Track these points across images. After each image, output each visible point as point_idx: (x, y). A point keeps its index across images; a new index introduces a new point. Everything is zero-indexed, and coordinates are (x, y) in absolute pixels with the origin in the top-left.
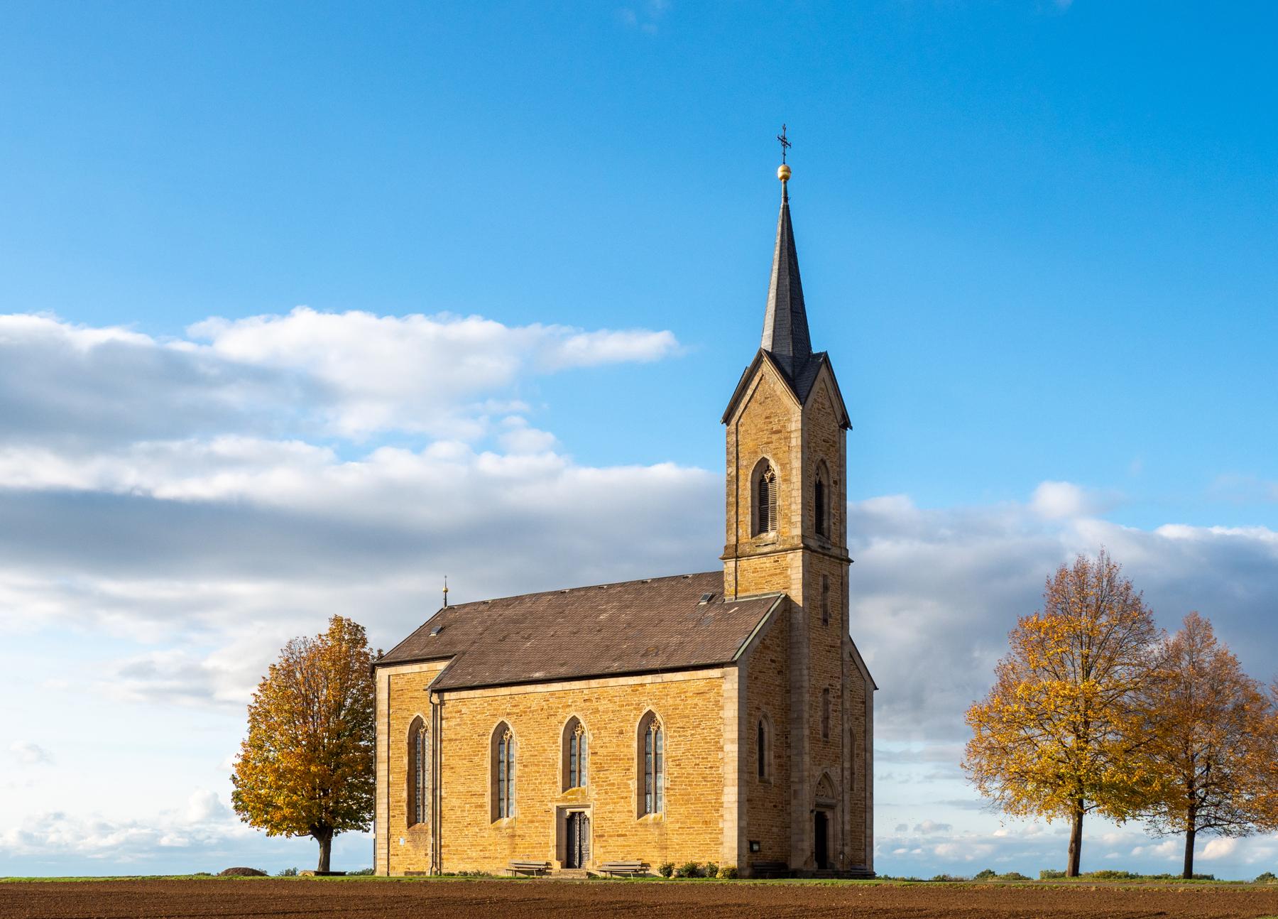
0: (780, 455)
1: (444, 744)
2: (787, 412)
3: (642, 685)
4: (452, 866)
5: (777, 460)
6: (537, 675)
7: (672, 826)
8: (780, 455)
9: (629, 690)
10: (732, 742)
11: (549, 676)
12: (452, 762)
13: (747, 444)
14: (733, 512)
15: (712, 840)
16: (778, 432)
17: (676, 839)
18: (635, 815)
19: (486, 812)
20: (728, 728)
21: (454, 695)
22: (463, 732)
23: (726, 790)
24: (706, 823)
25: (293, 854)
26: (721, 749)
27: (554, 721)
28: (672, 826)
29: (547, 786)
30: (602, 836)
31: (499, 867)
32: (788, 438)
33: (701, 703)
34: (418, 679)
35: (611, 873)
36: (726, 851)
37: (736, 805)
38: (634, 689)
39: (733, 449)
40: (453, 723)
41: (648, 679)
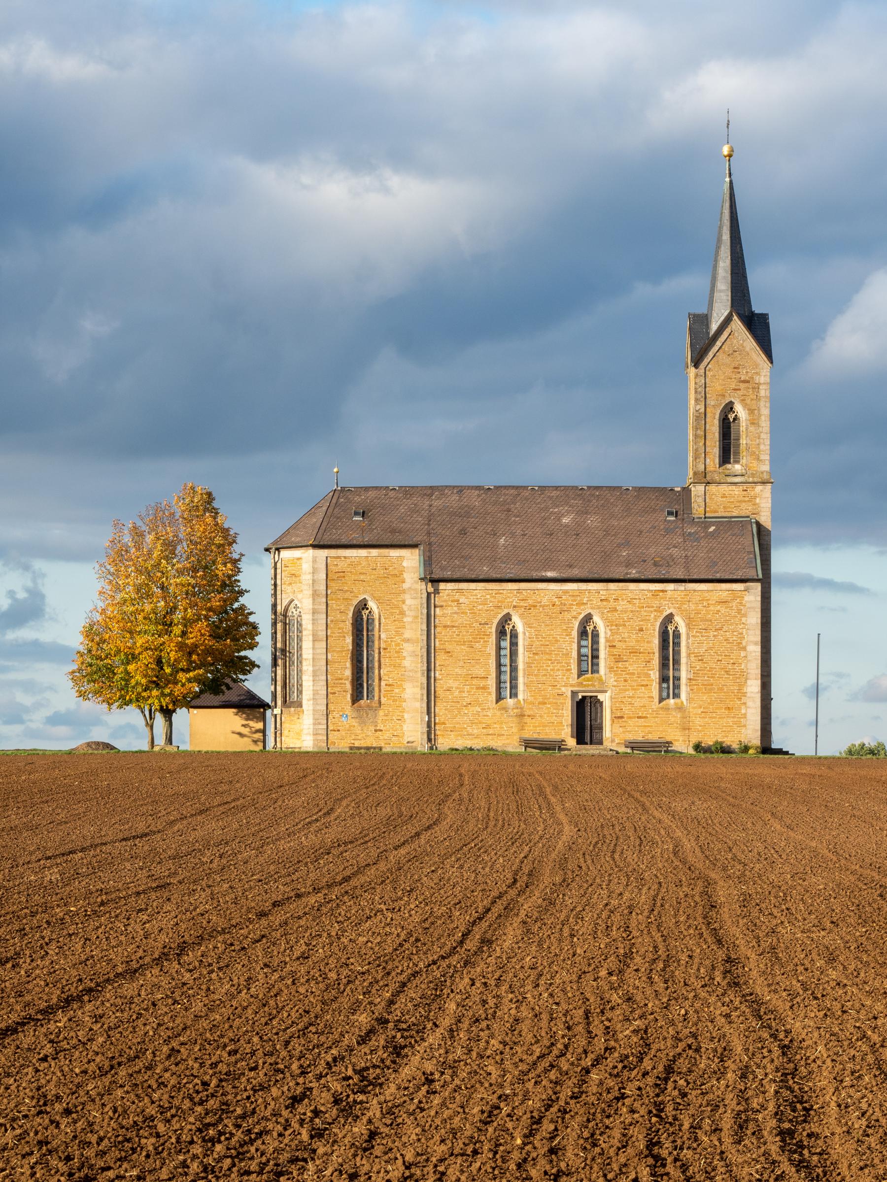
0: (748, 401)
1: (438, 630)
2: (756, 366)
3: (663, 591)
4: (444, 743)
6: (550, 574)
7: (695, 711)
8: (748, 401)
9: (649, 595)
10: (756, 644)
11: (564, 576)
12: (449, 647)
14: (702, 444)
15: (735, 723)
17: (698, 721)
18: (657, 700)
19: (490, 693)
20: (750, 632)
21: (450, 586)
22: (460, 620)
23: (749, 682)
25: (126, 728)
26: (744, 649)
27: (567, 616)
28: (695, 711)
29: (560, 673)
30: (622, 717)
31: (508, 741)
32: (756, 388)
33: (723, 610)
34: (364, 564)
35: (632, 748)
36: (749, 732)
37: (759, 695)
38: (655, 594)
39: (701, 390)
40: (449, 611)
41: (671, 586)
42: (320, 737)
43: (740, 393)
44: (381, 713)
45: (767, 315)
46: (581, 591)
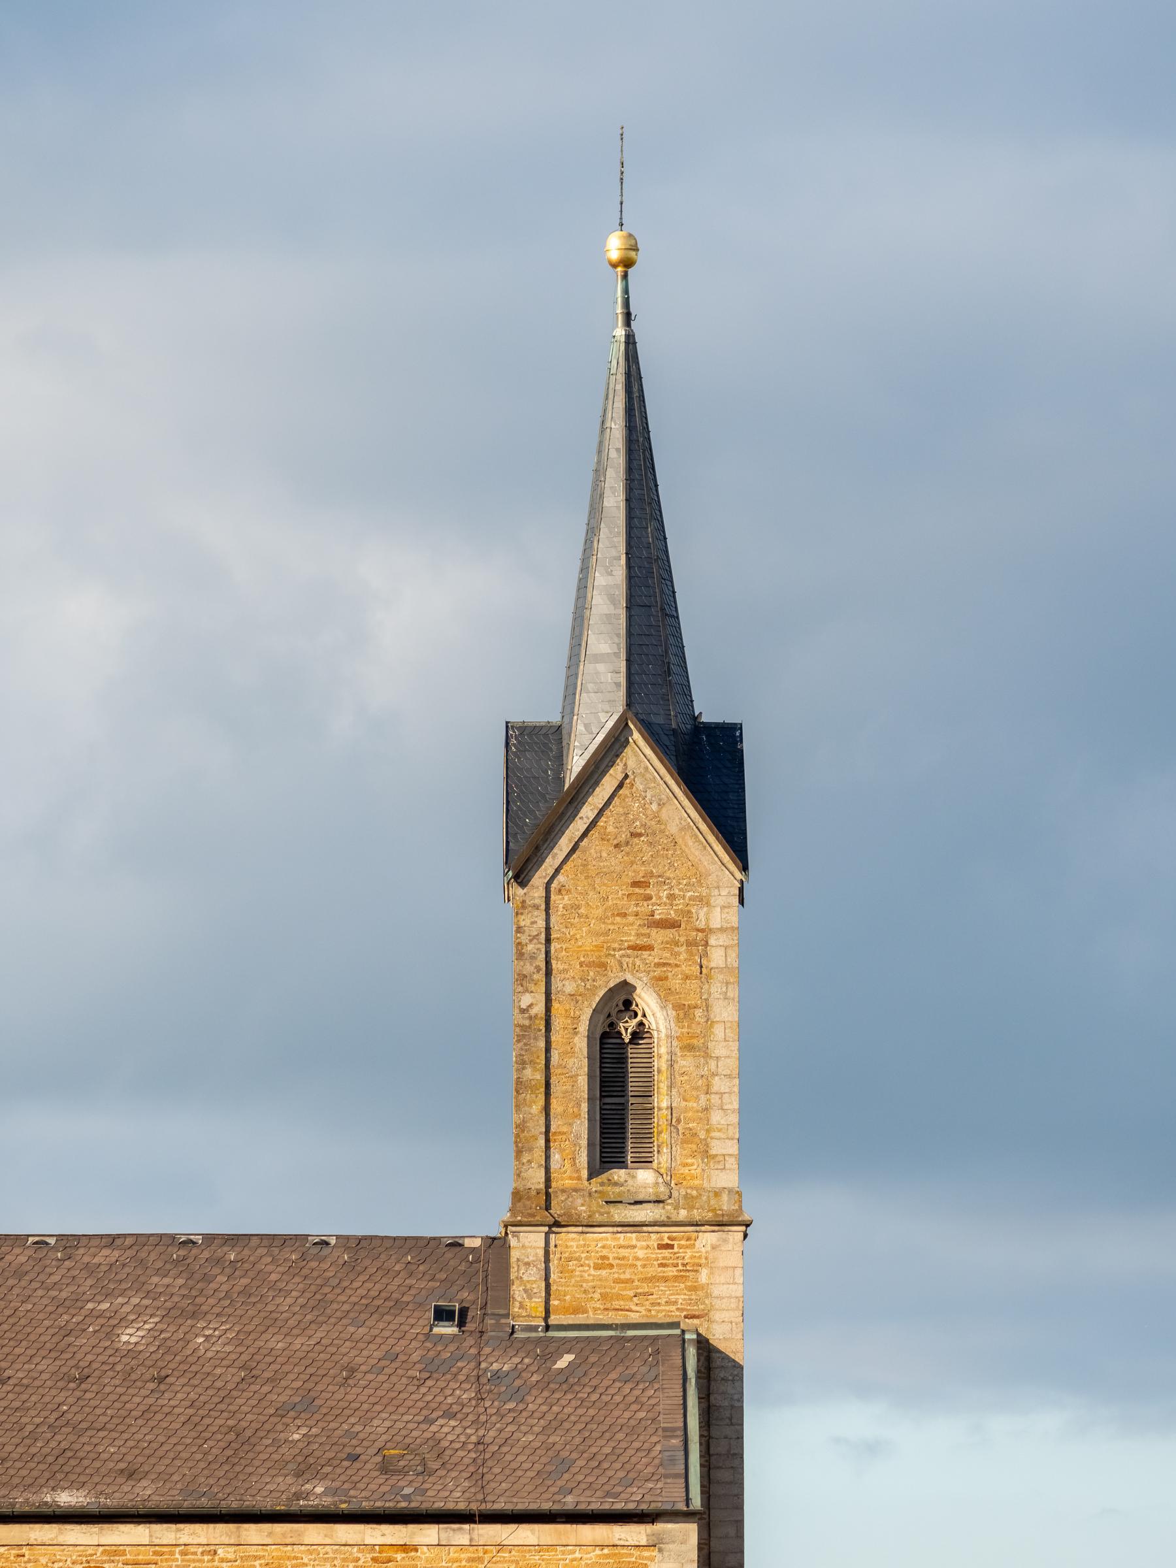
0: (675, 983)
3: (405, 1548)
5: (665, 994)
6: (66, 1499)
8: (675, 983)
11: (110, 1503)
13: (577, 941)
14: (537, 1107)
16: (673, 925)
32: (700, 943)
39: (535, 948)
41: (429, 1534)
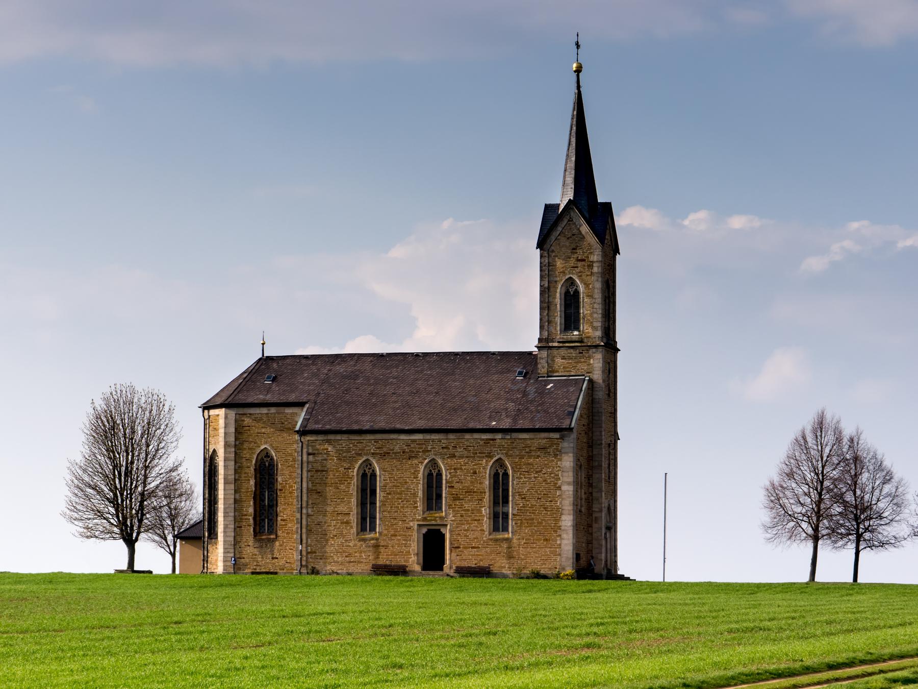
9: (482, 443)
10: (569, 484)
20: (565, 474)
23: (563, 517)
24: (546, 540)
32: (590, 266)
38: (487, 442)
42: (229, 564)
43: (578, 270)
44: (277, 543)
45: (546, 205)
46: (427, 441)
